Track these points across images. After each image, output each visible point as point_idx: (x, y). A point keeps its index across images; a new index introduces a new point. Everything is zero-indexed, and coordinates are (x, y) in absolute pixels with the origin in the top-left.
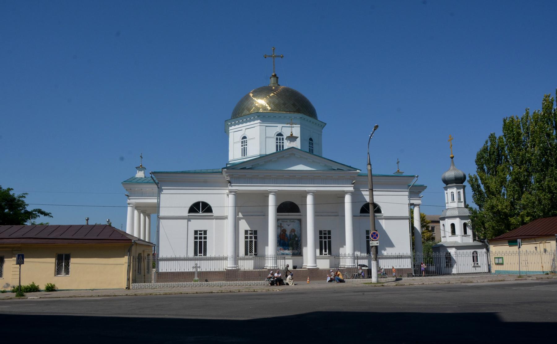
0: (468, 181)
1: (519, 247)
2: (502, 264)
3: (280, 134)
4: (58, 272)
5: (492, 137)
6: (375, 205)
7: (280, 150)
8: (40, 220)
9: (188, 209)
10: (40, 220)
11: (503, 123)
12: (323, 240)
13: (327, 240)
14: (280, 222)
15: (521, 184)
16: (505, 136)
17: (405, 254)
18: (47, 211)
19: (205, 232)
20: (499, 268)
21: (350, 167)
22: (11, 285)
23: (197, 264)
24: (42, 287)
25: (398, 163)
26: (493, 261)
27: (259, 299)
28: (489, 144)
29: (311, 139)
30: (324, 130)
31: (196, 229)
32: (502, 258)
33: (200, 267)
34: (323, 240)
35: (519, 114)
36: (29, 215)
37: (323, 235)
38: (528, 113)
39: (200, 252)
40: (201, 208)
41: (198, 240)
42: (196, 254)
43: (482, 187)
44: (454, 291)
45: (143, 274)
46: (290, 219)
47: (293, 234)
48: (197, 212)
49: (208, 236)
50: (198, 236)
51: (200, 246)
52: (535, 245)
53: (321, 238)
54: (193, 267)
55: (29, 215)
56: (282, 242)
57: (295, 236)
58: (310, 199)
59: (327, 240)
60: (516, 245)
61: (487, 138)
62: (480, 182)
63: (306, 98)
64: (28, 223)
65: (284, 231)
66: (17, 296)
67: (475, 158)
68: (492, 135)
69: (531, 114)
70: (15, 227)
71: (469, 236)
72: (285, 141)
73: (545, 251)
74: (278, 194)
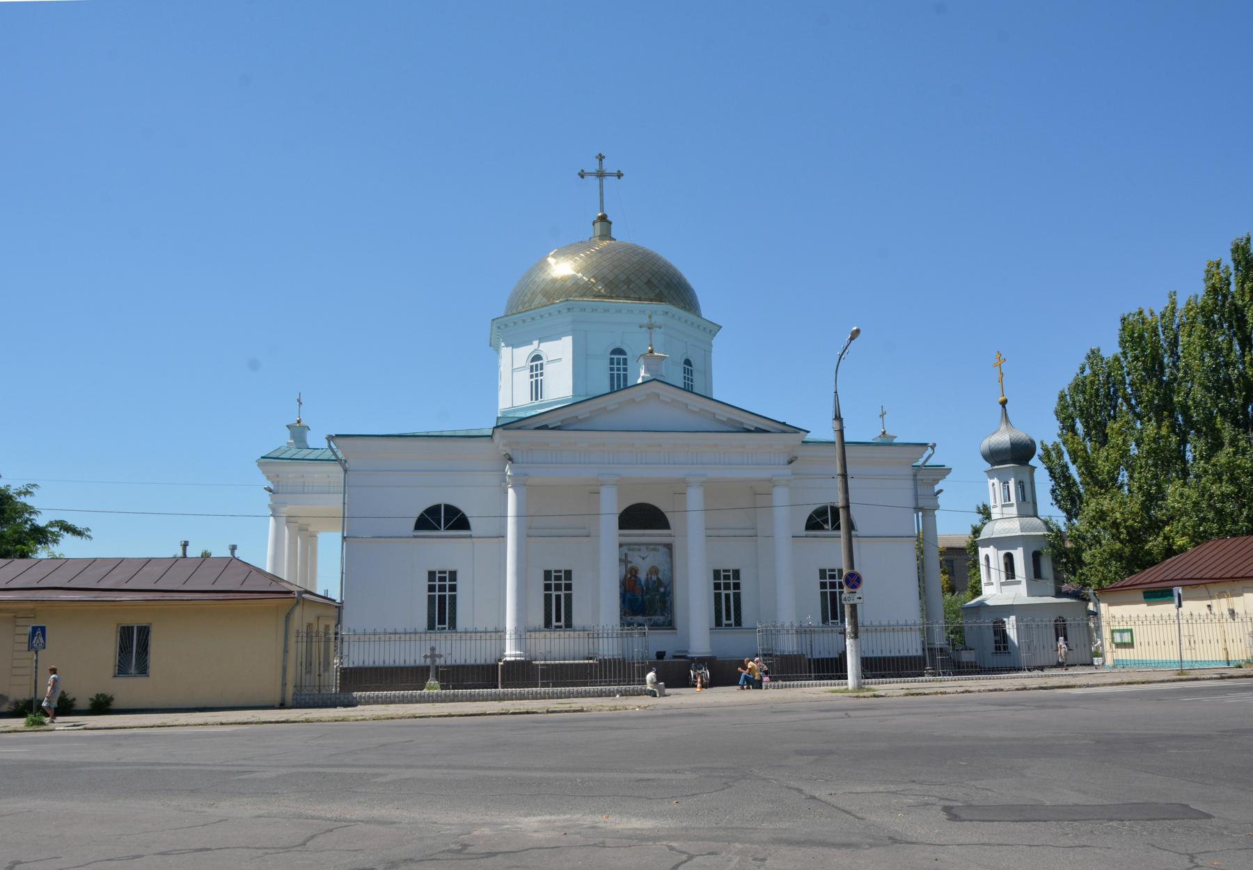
0: (1040, 458)
1: (1180, 606)
2: (1130, 645)
4: (122, 670)
5: (1094, 355)
7: (619, 385)
8: (68, 547)
9: (413, 521)
10: (68, 547)
11: (1120, 326)
12: (554, 593)
13: (731, 592)
14: (625, 549)
15: (1168, 460)
16: (1124, 354)
18: (79, 525)
20: (1123, 654)
21: (784, 424)
22: (12, 699)
23: (433, 649)
24: (83, 702)
25: (882, 416)
27: (1063, 707)
28: (1088, 372)
29: (688, 362)
31: (432, 569)
32: (1131, 631)
34: (723, 592)
35: (1155, 306)
36: (40, 535)
37: (553, 582)
38: (1174, 303)
41: (437, 593)
43: (1073, 470)
44: (1054, 707)
46: (647, 544)
47: (654, 578)
48: (435, 529)
50: (437, 583)
51: (442, 608)
52: (1209, 602)
53: (717, 586)
54: (426, 657)
55: (40, 535)
56: (628, 595)
57: (659, 583)
58: (695, 498)
59: (562, 593)
60: (1172, 602)
61: (1084, 361)
62: (1067, 458)
63: (671, 266)
64: (42, 553)
65: (633, 572)
66: (28, 725)
67: (1054, 403)
68: (1093, 352)
69: (1181, 305)
70: (18, 564)
71: (1019, 583)
73: (1232, 613)
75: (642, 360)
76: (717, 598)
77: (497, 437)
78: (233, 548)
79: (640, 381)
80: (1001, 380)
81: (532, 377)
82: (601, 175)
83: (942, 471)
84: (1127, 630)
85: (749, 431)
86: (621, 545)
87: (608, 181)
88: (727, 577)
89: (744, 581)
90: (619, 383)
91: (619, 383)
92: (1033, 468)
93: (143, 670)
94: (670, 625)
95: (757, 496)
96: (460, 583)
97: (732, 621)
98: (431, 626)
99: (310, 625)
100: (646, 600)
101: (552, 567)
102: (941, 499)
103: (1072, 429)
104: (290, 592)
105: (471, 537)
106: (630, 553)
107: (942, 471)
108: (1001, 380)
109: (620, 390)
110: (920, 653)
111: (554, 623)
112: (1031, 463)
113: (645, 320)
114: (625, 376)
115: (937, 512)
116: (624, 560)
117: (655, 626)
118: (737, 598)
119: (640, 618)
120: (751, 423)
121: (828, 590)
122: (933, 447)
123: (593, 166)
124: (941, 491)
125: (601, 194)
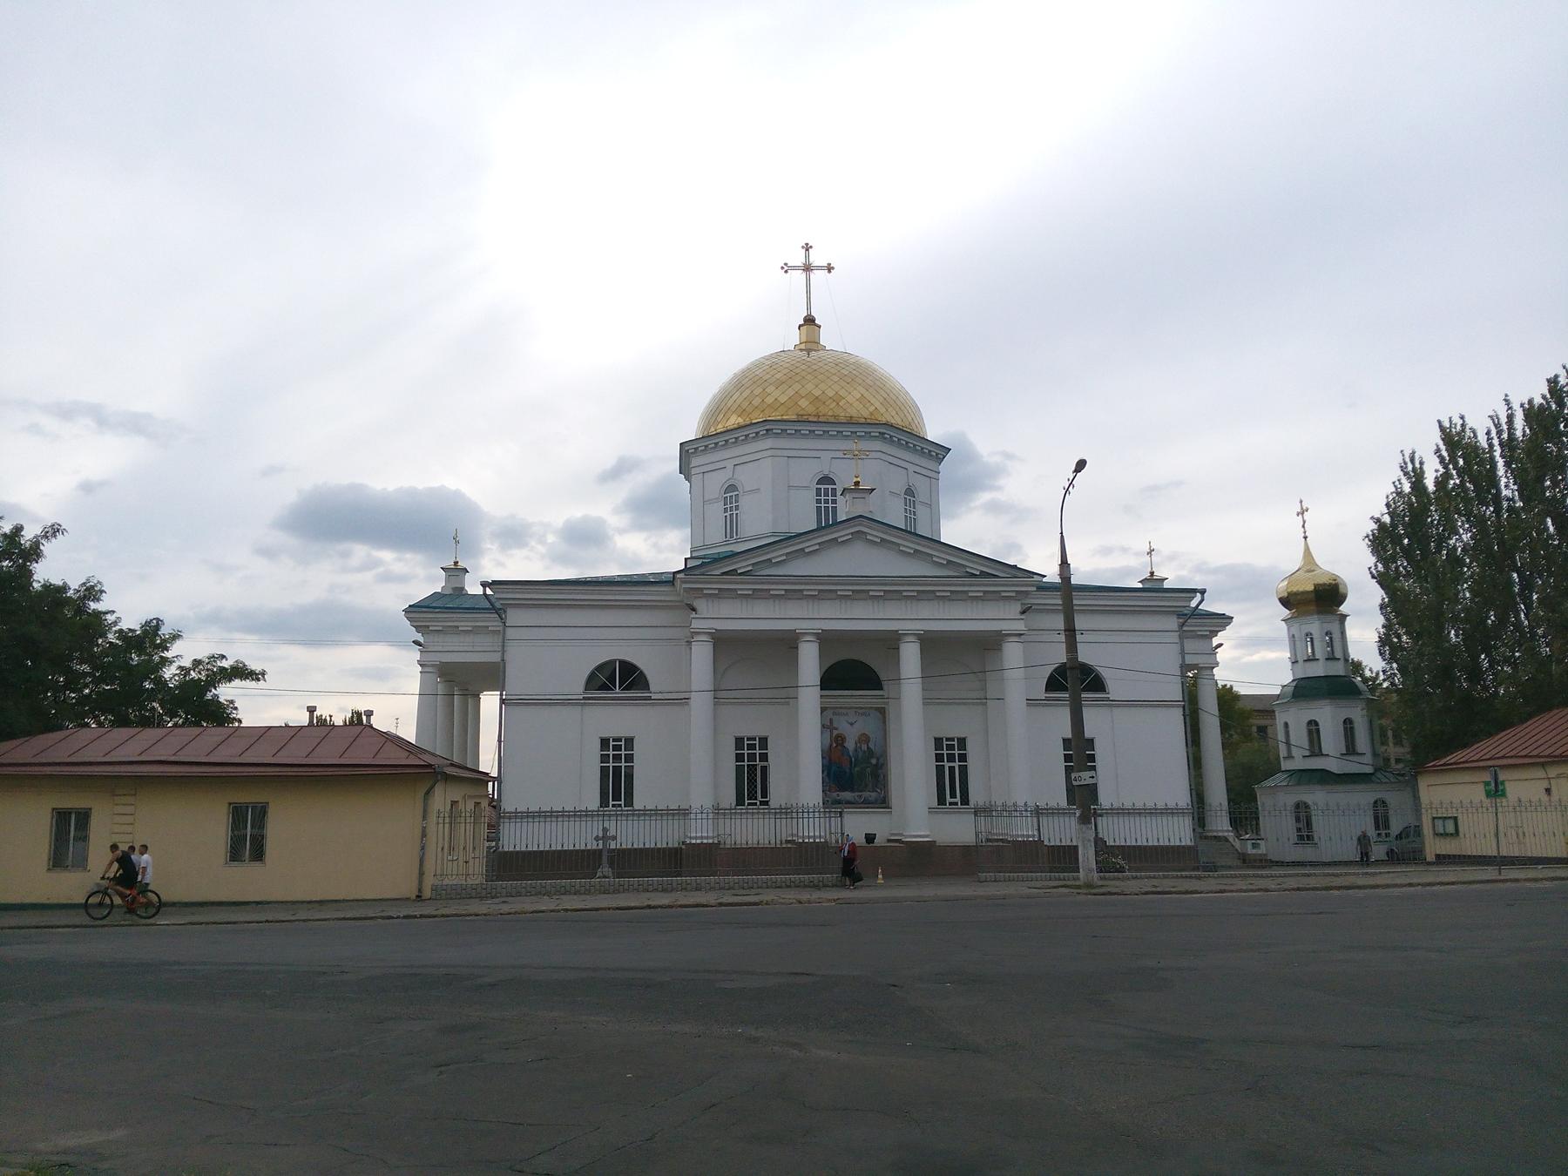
3: (826, 480)
6: (1086, 670)
7: (827, 519)
12: (947, 765)
13: (956, 764)
14: (829, 713)
17: (1053, 804)
23: (605, 830)
33: (614, 838)
34: (947, 765)
37: (611, 753)
39: (617, 797)
40: (618, 679)
42: (604, 802)
49: (771, 752)
53: (939, 758)
54: (597, 839)
57: (870, 753)
58: (910, 656)
59: (956, 764)
63: (757, 365)
65: (840, 740)
72: (839, 498)
74: (826, 640)
76: (940, 771)
82: (807, 268)
86: (823, 710)
87: (816, 276)
88: (951, 747)
89: (972, 750)
93: (258, 854)
94: (883, 803)
95: (983, 648)
96: (637, 752)
97: (958, 799)
98: (740, 801)
100: (855, 774)
101: (745, 732)
102: (1221, 655)
104: (430, 766)
105: (649, 698)
106: (835, 718)
107: (1224, 620)
109: (828, 526)
116: (827, 727)
117: (867, 804)
118: (964, 771)
119: (847, 795)
120: (976, 568)
122: (1203, 592)
125: (808, 292)
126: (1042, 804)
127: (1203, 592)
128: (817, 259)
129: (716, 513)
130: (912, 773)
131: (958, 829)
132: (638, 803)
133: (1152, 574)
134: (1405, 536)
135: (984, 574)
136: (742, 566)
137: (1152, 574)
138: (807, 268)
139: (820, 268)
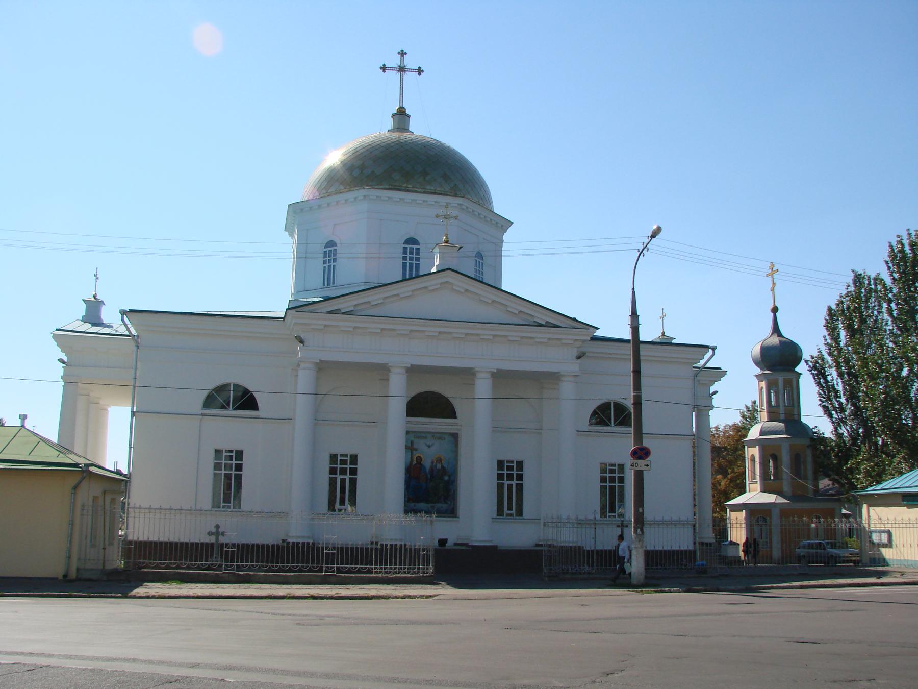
7: (411, 274)
12: (506, 483)
17: (684, 518)
19: (240, 454)
21: (574, 319)
23: (218, 527)
26: (426, 531)
30: (506, 237)
31: (501, 458)
37: (506, 472)
39: (342, 502)
45: (102, 546)
48: (606, 424)
49: (359, 467)
53: (500, 477)
54: (210, 534)
57: (444, 470)
58: (483, 386)
74: (413, 371)
75: (437, 250)
76: (500, 487)
77: (288, 319)
78: (23, 418)
79: (434, 270)
80: (773, 290)
81: (325, 262)
82: (402, 69)
83: (718, 373)
84: (884, 531)
85: (540, 325)
86: (408, 433)
87: (408, 76)
89: (527, 472)
90: (412, 272)
91: (412, 272)
92: (799, 374)
94: (452, 512)
99: (95, 498)
100: (429, 487)
102: (716, 400)
103: (836, 339)
104: (77, 465)
107: (718, 373)
108: (773, 290)
109: (411, 278)
110: (691, 548)
111: (506, 511)
112: (797, 369)
113: (441, 212)
114: (418, 266)
115: (711, 413)
116: (410, 448)
117: (440, 513)
118: (520, 488)
119: (422, 505)
120: (542, 318)
121: (608, 484)
122: (714, 349)
123: (395, 62)
124: (716, 392)
126: (582, 517)
127: (714, 349)
128: (409, 62)
129: (317, 267)
130: (476, 486)
131: (517, 535)
132: (245, 505)
133: (663, 334)
134: (851, 315)
135: (548, 325)
136: (345, 304)
137: (663, 334)
138: (402, 69)
139: (412, 70)
